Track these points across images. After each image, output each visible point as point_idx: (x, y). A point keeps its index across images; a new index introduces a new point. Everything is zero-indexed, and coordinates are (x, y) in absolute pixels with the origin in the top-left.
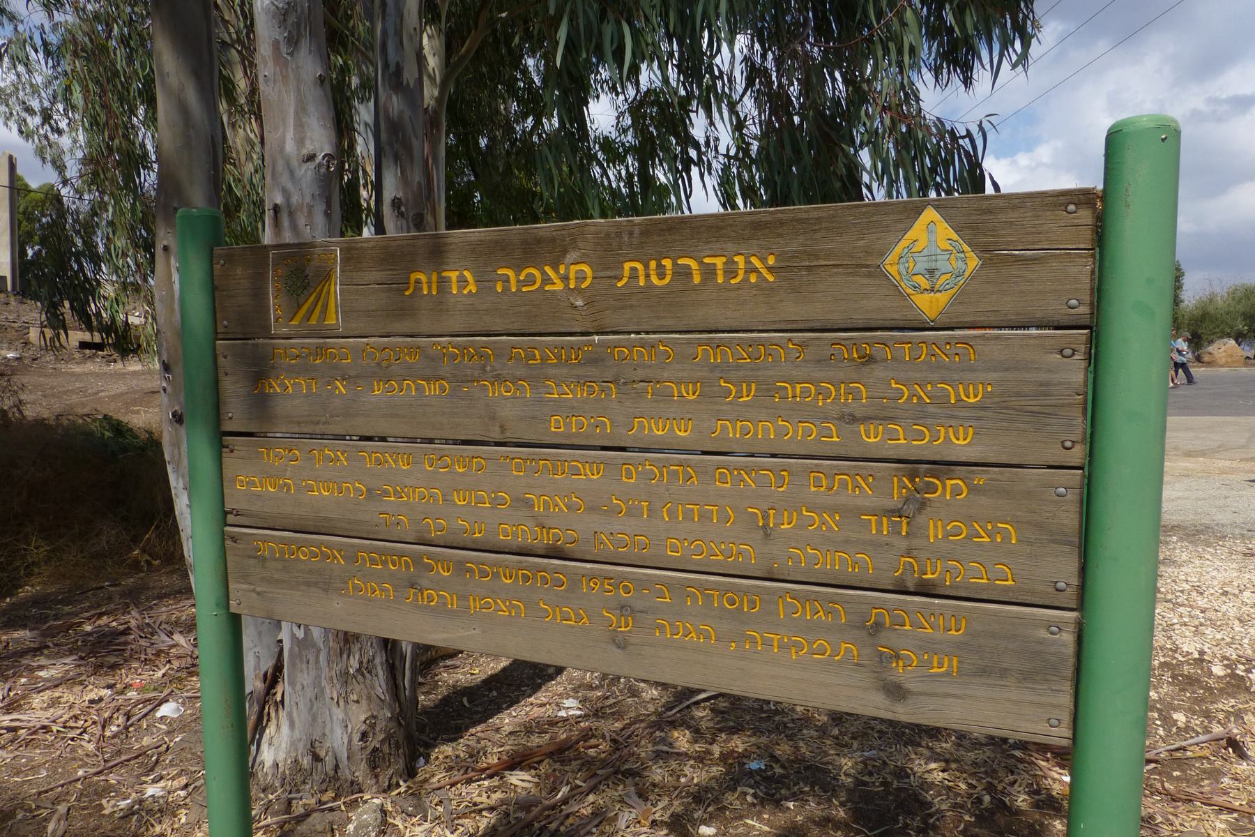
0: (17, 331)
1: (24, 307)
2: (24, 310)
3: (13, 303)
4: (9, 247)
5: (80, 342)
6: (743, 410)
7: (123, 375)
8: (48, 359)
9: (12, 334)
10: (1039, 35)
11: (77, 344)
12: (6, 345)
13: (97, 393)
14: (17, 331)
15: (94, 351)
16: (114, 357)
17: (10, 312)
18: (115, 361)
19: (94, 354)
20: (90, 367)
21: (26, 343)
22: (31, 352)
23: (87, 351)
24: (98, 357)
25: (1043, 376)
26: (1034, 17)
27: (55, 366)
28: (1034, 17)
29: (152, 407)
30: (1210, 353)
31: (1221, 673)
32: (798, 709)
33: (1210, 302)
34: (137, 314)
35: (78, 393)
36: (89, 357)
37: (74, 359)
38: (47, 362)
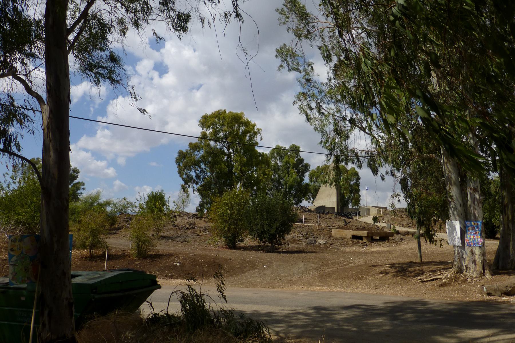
0: (327, 230)
1: (337, 220)
2: (336, 221)
6: (502, 320)
7: (366, 253)
9: (325, 232)
10: (394, 119)
11: (351, 237)
12: (322, 237)
13: (348, 264)
14: (327, 230)
15: (358, 240)
16: (367, 243)
18: (367, 246)
20: (355, 248)
22: (331, 241)
23: (355, 240)
24: (359, 243)
25: (198, 336)
26: (31, 119)
27: (339, 248)
28: (31, 119)
29: (370, 276)
34: (384, 222)
38: (337, 246)
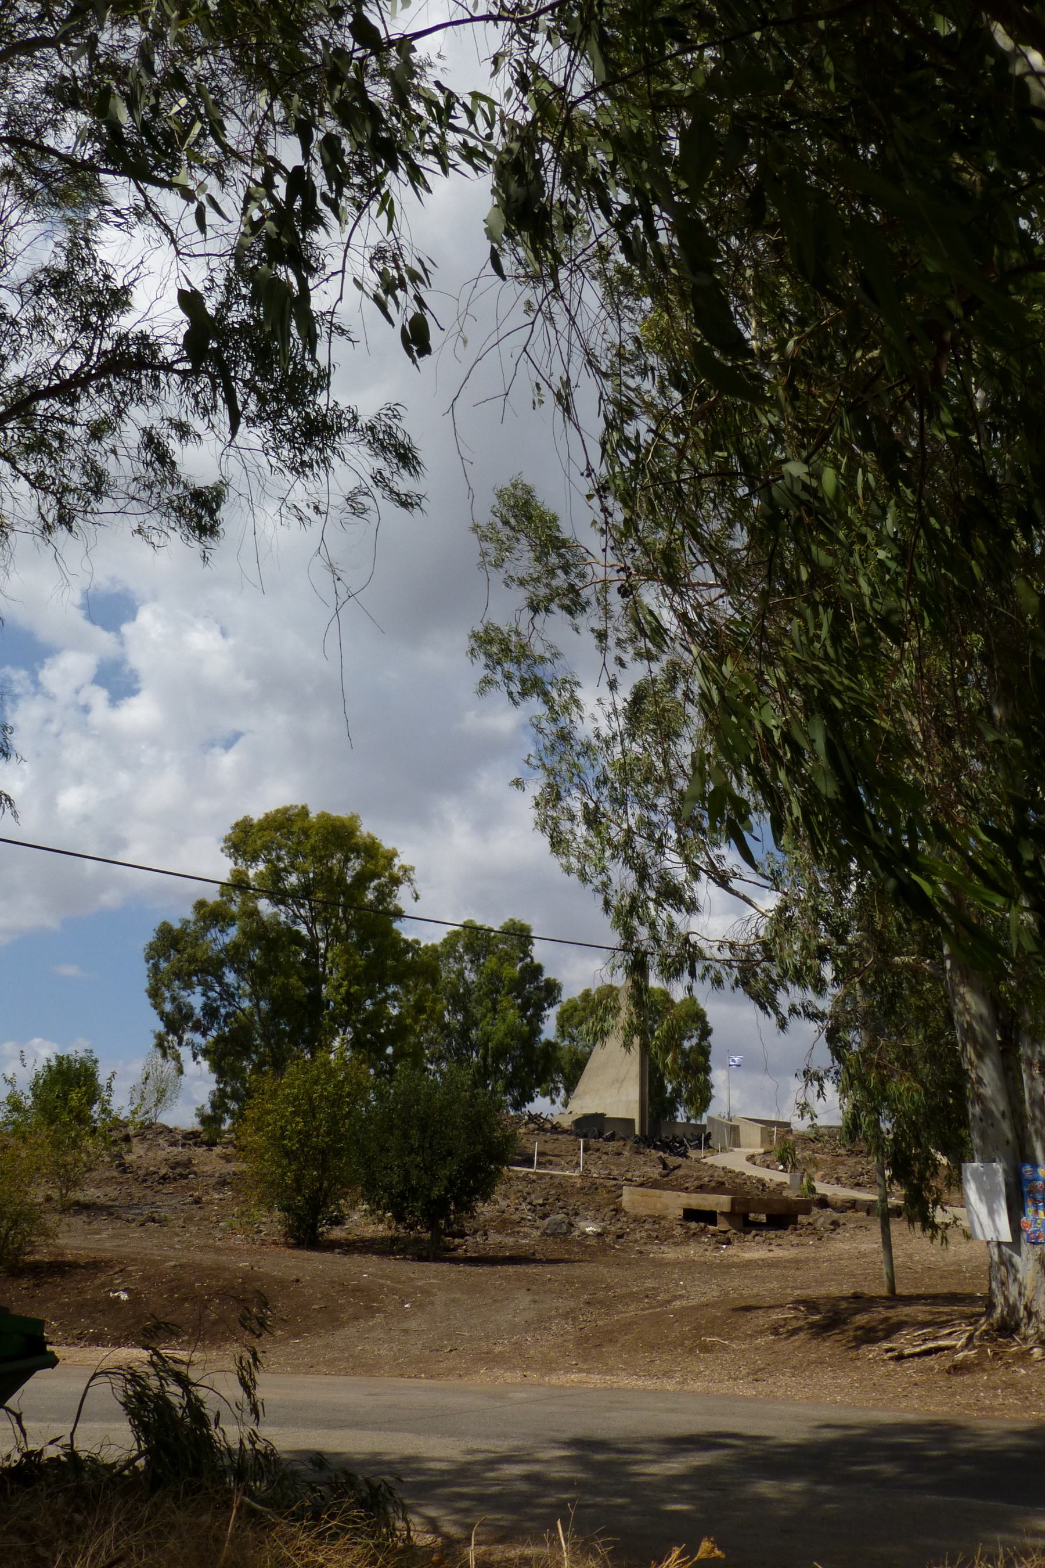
0: (609, 1192)
3: (626, 1153)
4: (638, 1080)
5: (685, 1210)
7: (726, 1267)
8: (638, 1236)
11: (681, 1212)
12: (591, 1213)
13: (669, 1302)
15: (702, 1224)
17: (618, 1165)
18: (728, 1242)
19: (702, 1230)
21: (618, 1210)
23: (693, 1225)
29: (738, 1338)
30: (180, 1071)
31: (728, 675)
32: (242, 229)
33: (246, 832)
35: (641, 1301)
36: (694, 1234)
37: (673, 1236)
